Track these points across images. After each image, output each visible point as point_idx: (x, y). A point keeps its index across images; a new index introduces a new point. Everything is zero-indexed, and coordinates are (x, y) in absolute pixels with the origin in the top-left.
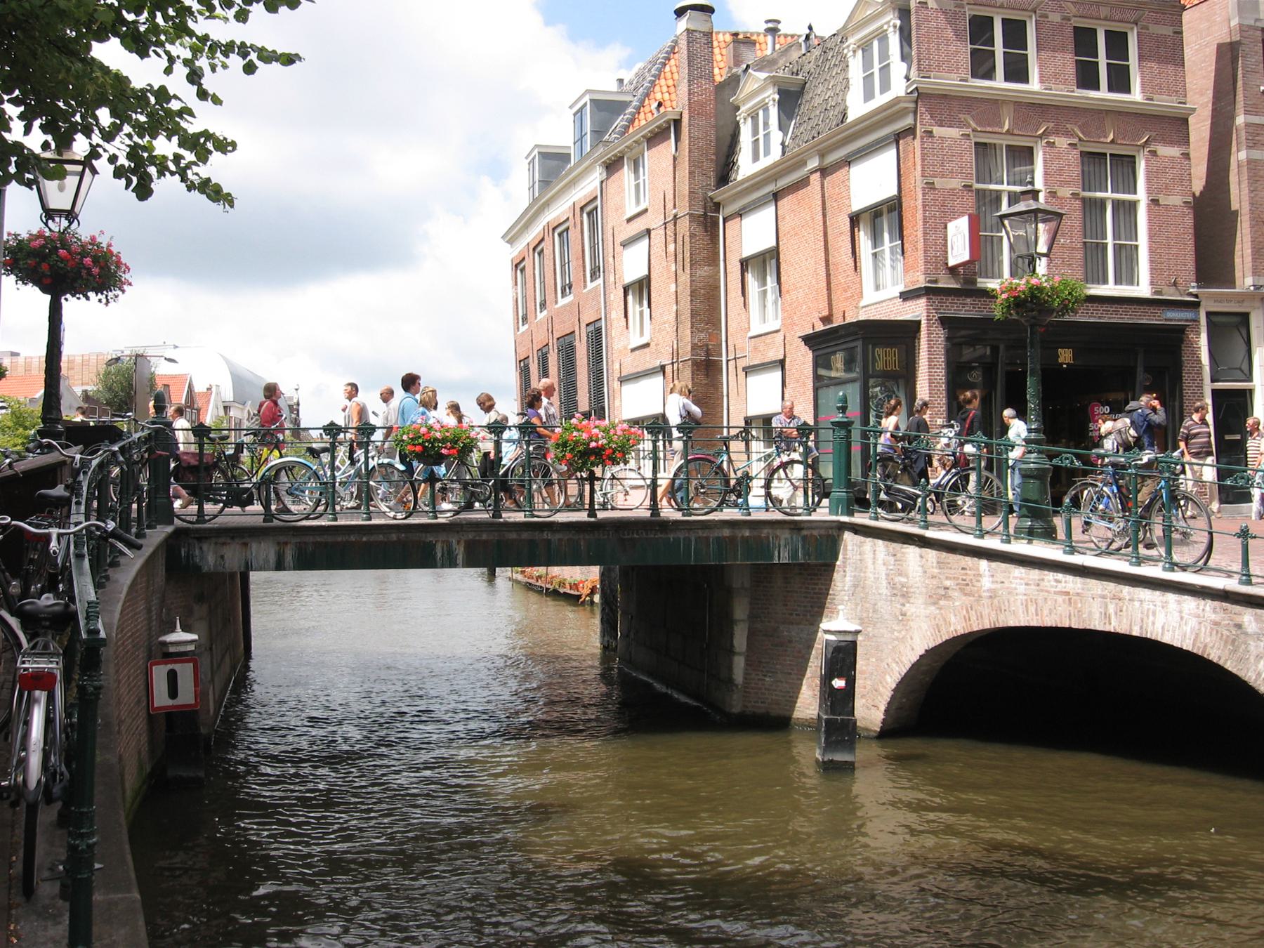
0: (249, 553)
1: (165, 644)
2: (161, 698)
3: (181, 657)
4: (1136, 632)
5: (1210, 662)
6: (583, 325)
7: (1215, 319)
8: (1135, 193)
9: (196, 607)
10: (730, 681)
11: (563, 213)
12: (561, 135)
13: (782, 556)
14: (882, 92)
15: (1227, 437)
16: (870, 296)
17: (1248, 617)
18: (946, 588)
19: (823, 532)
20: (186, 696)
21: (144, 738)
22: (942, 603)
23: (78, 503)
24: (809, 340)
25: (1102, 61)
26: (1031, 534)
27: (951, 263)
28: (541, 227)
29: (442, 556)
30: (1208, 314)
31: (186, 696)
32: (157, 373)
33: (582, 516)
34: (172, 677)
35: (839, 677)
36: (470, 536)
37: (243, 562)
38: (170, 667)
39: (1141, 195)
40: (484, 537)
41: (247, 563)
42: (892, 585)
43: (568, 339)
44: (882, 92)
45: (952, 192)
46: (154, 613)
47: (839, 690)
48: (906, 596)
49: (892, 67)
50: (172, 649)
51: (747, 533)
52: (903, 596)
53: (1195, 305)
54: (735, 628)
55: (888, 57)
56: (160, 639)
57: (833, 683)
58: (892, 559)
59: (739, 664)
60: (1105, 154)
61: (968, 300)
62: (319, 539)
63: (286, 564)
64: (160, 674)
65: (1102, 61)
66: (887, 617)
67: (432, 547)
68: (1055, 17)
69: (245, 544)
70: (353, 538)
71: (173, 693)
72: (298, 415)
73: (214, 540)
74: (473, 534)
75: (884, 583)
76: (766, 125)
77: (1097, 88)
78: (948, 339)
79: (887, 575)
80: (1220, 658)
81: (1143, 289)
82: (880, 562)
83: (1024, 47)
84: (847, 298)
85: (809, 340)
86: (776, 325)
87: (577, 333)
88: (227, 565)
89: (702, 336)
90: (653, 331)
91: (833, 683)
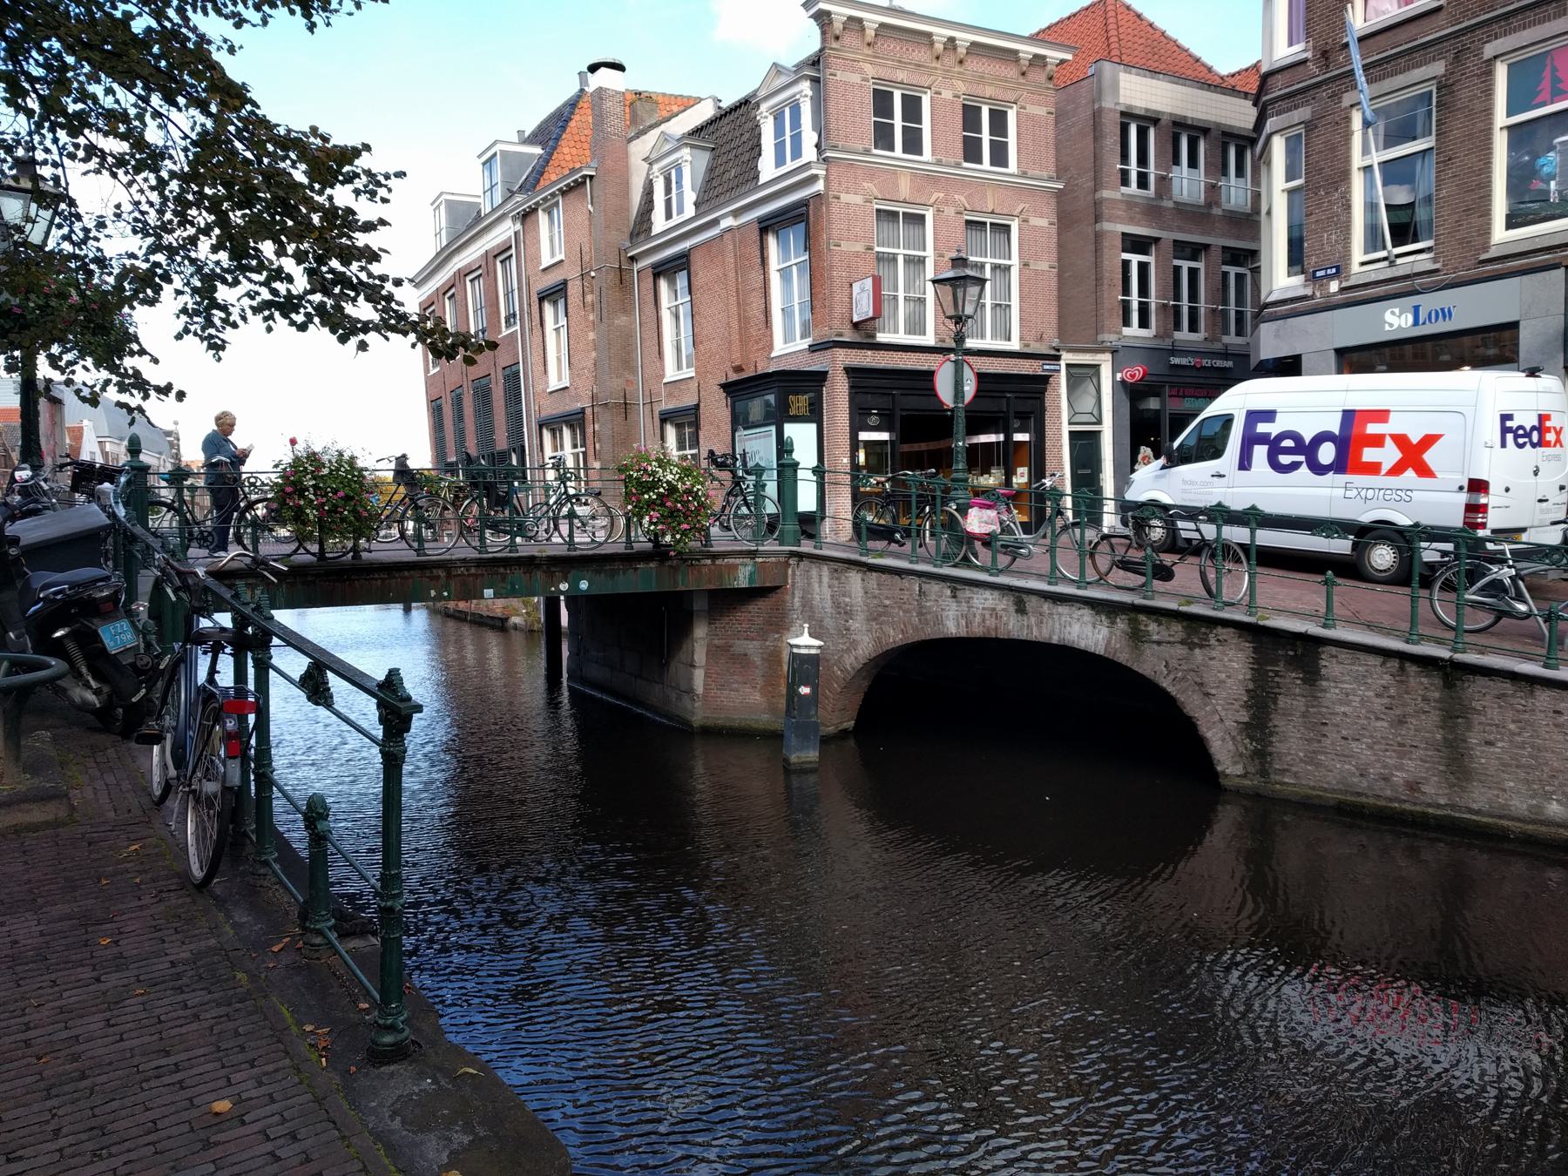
4: (1055, 640)
5: (1120, 664)
6: (499, 369)
7: (1073, 371)
8: (924, 250)
10: (690, 691)
11: (475, 261)
12: (471, 184)
14: (792, 160)
15: (1089, 471)
16: (780, 347)
24: (727, 387)
25: (986, 136)
26: (946, 558)
27: (855, 319)
28: (451, 273)
30: (1068, 365)
32: (316, 450)
35: (806, 686)
39: (1015, 261)
42: (837, 605)
43: (484, 381)
44: (792, 160)
45: (857, 255)
47: (805, 695)
48: (849, 614)
49: (804, 135)
52: (846, 613)
53: (1058, 358)
55: (799, 126)
59: (699, 677)
60: (985, 223)
61: (869, 353)
65: (986, 136)
66: (832, 631)
68: (947, 94)
72: (178, 450)
75: (829, 602)
76: (679, 183)
77: (980, 161)
78: (851, 387)
79: (832, 596)
81: (1015, 345)
83: (891, 117)
84: (758, 350)
85: (727, 387)
86: (691, 373)
87: (493, 376)
90: (571, 377)
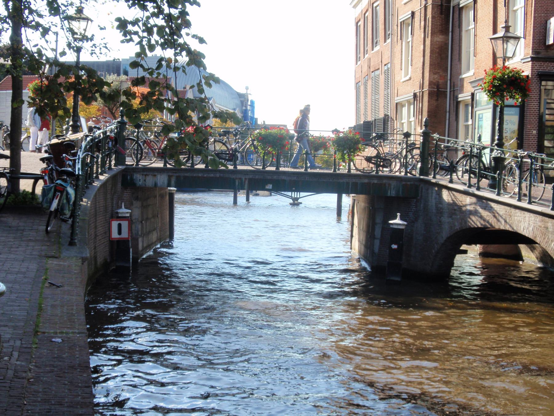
0: (156, 179)
1: (117, 213)
2: (115, 235)
3: (124, 218)
9: (134, 202)
13: (392, 193)
17: (550, 223)
18: (455, 210)
19: (412, 183)
20: (125, 234)
21: (107, 249)
22: (453, 216)
23: (81, 151)
29: (238, 185)
31: (125, 234)
33: (303, 170)
34: (120, 226)
35: (395, 244)
36: (251, 177)
37: (154, 183)
38: (119, 222)
40: (257, 177)
41: (155, 184)
46: (115, 201)
50: (120, 215)
51: (376, 182)
54: (376, 226)
56: (117, 211)
57: (392, 246)
58: (438, 196)
62: (186, 175)
63: (172, 185)
64: (115, 224)
67: (234, 180)
69: (155, 175)
70: (200, 175)
71: (120, 232)
73: (142, 173)
74: (252, 176)
79: (436, 204)
80: (540, 241)
82: (433, 197)
88: (147, 184)
89: (436, 76)
91: (392, 246)
